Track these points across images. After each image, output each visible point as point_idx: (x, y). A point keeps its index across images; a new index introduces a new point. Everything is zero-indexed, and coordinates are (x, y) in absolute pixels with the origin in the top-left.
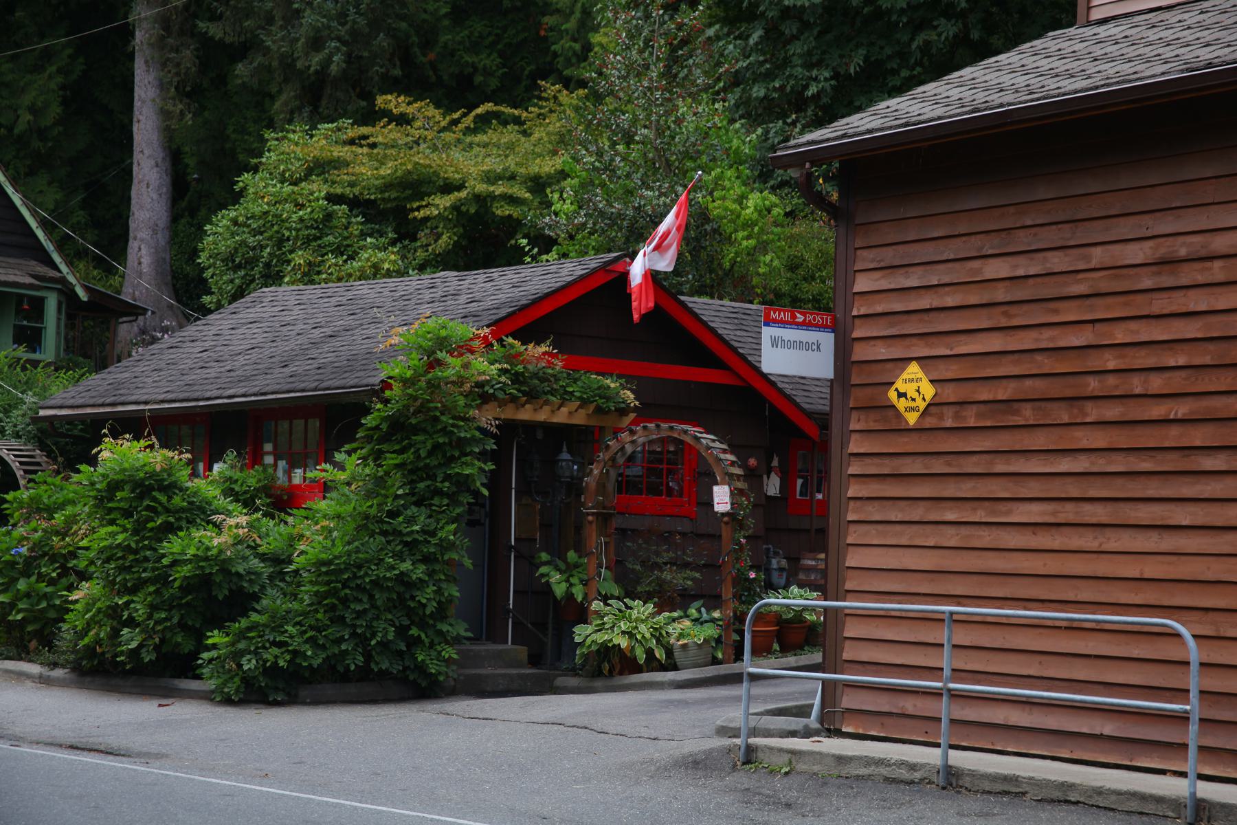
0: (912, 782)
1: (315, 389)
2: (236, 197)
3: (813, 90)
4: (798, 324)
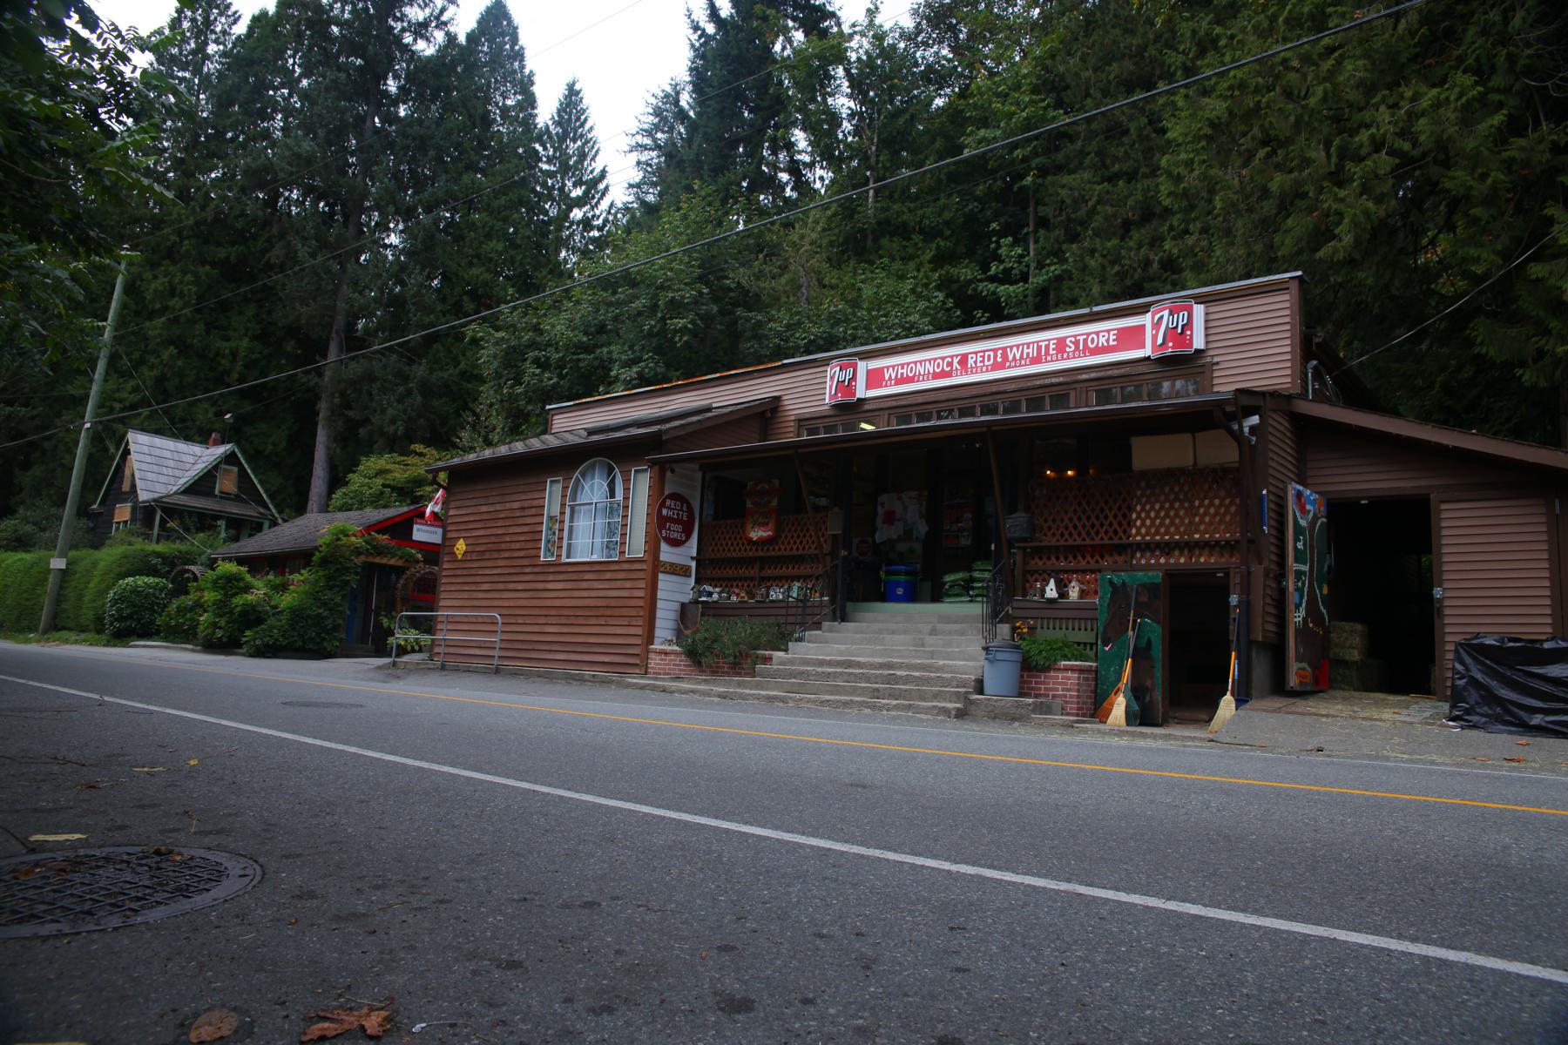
2: (346, 484)
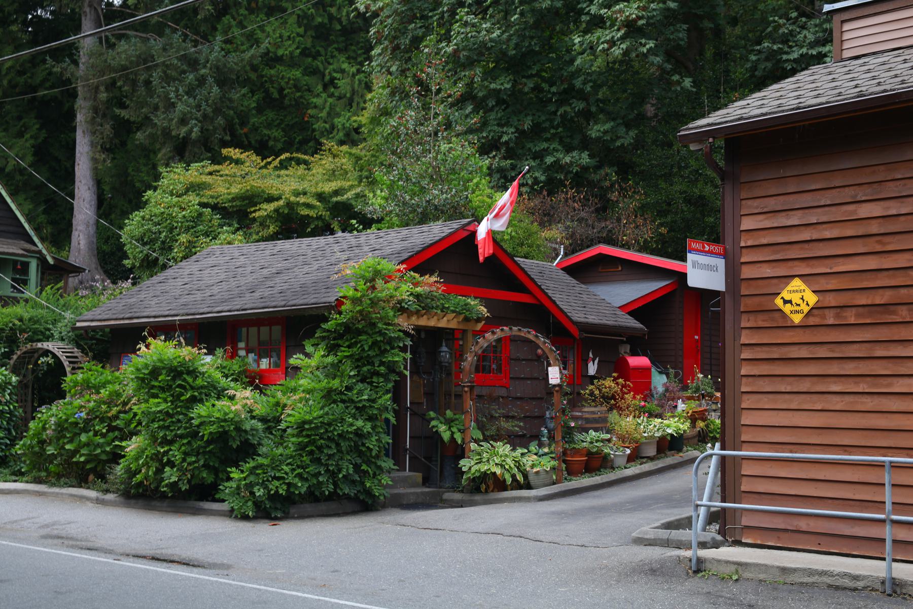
0: (855, 589)
1: (284, 306)
3: (505, 138)
4: (706, 252)
